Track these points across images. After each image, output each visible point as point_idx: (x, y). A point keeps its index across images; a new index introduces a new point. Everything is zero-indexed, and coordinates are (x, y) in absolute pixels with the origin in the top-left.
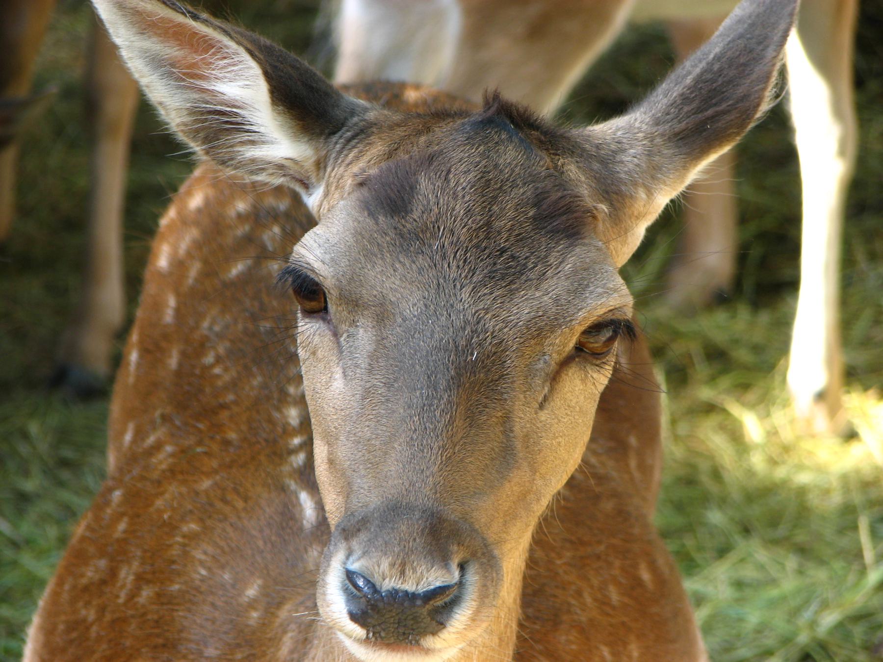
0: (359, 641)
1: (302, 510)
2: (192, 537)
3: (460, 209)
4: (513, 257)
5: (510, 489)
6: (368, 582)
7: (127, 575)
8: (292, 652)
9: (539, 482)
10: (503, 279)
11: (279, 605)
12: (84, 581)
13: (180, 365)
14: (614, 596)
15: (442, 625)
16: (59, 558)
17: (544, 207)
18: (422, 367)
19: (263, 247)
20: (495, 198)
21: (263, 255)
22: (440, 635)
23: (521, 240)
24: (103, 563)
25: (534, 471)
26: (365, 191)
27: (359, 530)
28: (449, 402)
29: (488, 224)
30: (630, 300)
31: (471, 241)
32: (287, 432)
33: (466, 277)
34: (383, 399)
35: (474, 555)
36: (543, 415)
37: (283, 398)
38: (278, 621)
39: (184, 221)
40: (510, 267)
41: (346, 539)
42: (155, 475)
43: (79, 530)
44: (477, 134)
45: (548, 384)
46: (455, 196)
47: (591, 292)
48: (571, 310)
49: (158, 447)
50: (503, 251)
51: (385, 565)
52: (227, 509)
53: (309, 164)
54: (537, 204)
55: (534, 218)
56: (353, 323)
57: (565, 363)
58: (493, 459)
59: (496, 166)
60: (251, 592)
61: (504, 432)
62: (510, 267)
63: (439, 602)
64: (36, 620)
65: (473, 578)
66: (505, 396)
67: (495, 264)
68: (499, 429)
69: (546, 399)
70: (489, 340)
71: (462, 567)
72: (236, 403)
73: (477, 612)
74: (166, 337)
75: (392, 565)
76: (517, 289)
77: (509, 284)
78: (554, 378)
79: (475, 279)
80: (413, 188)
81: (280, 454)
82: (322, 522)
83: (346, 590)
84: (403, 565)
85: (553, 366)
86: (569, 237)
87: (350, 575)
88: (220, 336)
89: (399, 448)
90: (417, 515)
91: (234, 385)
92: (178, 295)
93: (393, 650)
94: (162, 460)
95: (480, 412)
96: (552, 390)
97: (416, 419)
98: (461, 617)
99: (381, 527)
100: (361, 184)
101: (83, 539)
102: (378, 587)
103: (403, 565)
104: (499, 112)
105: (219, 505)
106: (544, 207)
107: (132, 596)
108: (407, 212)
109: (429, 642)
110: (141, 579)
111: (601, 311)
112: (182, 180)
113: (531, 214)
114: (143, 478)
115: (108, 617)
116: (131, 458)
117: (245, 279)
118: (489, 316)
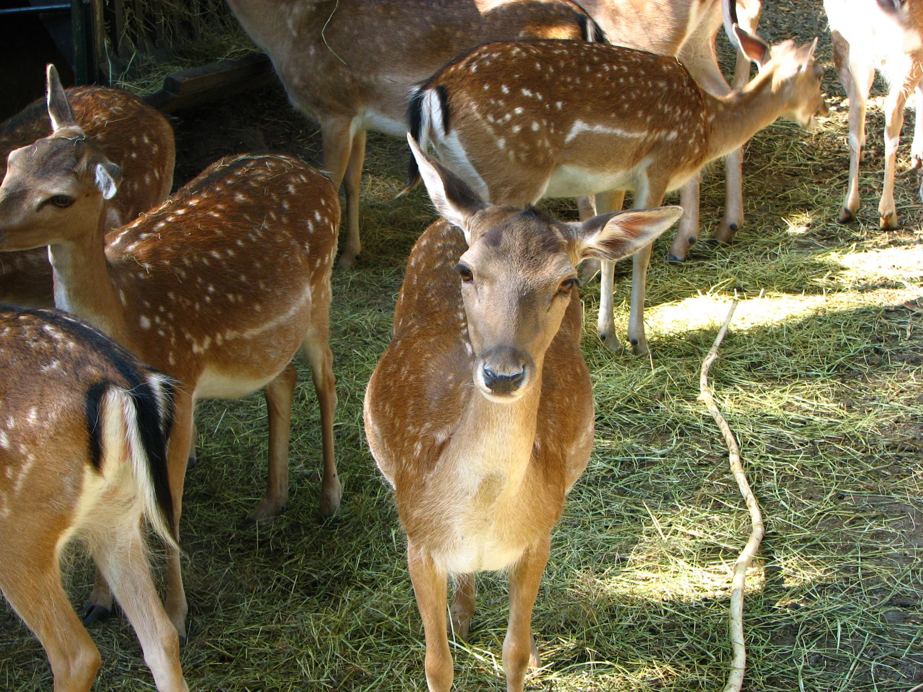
0: (489, 394)
1: (467, 350)
2: (428, 359)
3: (517, 244)
5: (538, 340)
6: (492, 373)
7: (404, 371)
8: (465, 398)
9: (547, 337)
11: (460, 382)
12: (389, 372)
13: (419, 298)
14: (569, 378)
15: (518, 387)
16: (378, 365)
19: (447, 257)
21: (447, 260)
24: (395, 366)
25: (546, 333)
26: (484, 238)
29: (527, 248)
30: (577, 273)
32: (459, 321)
35: (527, 362)
36: (549, 314)
37: (457, 310)
38: (460, 388)
39: (420, 250)
41: (483, 358)
42: (413, 335)
43: (384, 354)
46: (515, 239)
49: (413, 326)
50: (532, 258)
51: (498, 367)
52: (441, 349)
54: (543, 241)
55: (543, 246)
56: (482, 284)
57: (556, 295)
60: (450, 378)
63: (516, 380)
64: (369, 384)
65: (527, 371)
71: (524, 367)
72: (440, 311)
73: (529, 382)
74: (413, 289)
75: (500, 367)
78: (552, 301)
80: (501, 236)
81: (459, 329)
82: (474, 354)
83: (484, 376)
84: (504, 367)
85: (551, 297)
87: (485, 371)
88: (433, 288)
90: (508, 349)
91: (439, 304)
92: (418, 275)
94: (415, 330)
96: (551, 305)
98: (524, 384)
99: (496, 354)
100: (483, 236)
101: (387, 357)
103: (504, 367)
104: (530, 210)
105: (438, 348)
107: (406, 378)
109: (514, 393)
110: (410, 373)
112: (419, 236)
114: (408, 337)
115: (398, 385)
116: (403, 330)
117: (441, 268)
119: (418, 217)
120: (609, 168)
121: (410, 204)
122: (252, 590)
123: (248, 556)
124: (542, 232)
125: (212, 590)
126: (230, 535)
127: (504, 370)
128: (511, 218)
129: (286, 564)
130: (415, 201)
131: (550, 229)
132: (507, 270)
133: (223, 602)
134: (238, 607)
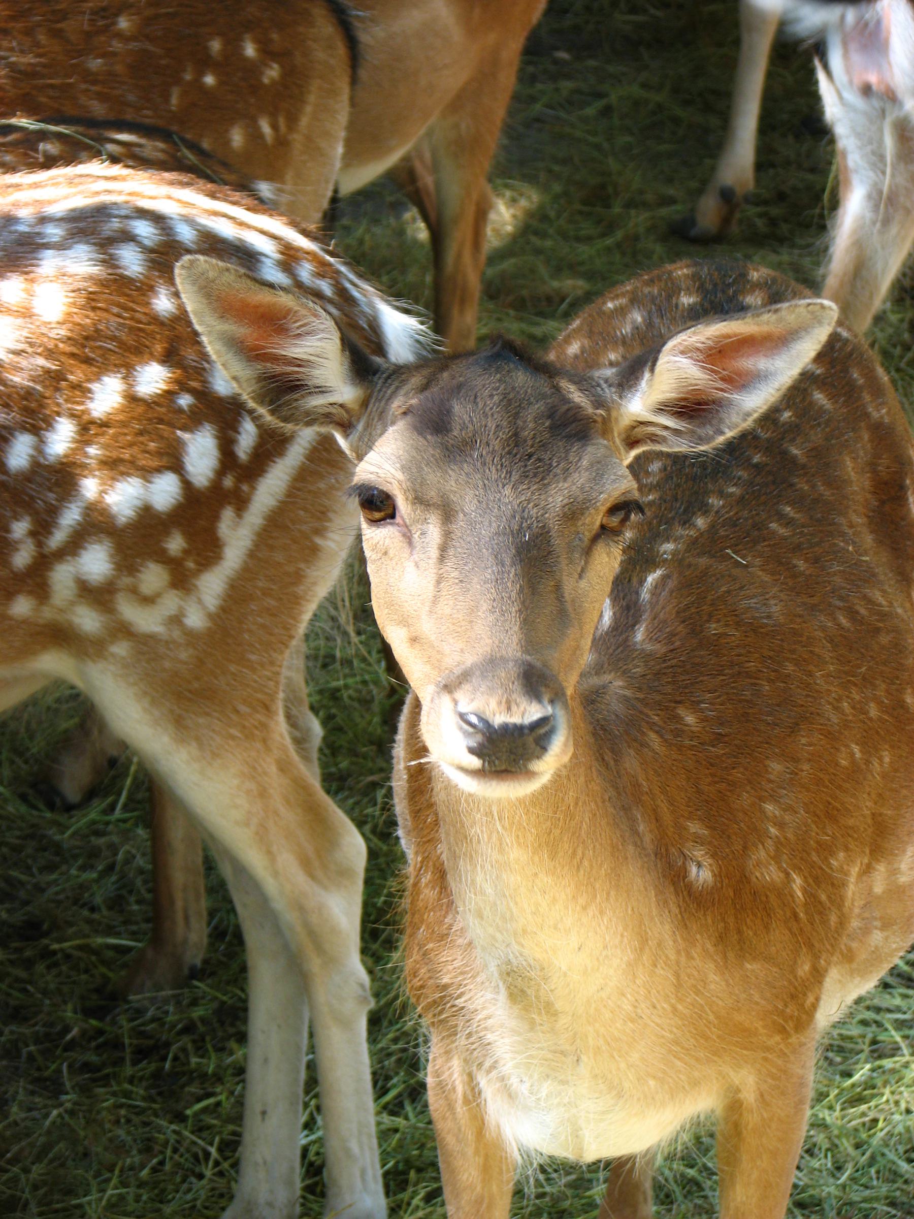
3: (492, 425)
4: (539, 460)
6: (481, 719)
10: (535, 476)
15: (544, 749)
17: (557, 418)
18: (487, 550)
20: (517, 414)
22: (544, 758)
23: (543, 446)
26: (409, 418)
27: (460, 683)
28: (516, 575)
29: (516, 434)
31: (504, 449)
33: (505, 478)
34: (457, 581)
36: (583, 584)
40: (539, 467)
44: (490, 366)
45: (584, 557)
47: (607, 479)
48: (594, 495)
50: (530, 456)
53: (354, 406)
54: (550, 417)
55: (551, 427)
57: (595, 539)
58: (553, 620)
59: (513, 388)
61: (557, 599)
62: (539, 467)
63: (542, 731)
66: (554, 569)
67: (526, 466)
68: (553, 596)
69: (583, 570)
70: (535, 525)
75: (499, 703)
76: (549, 484)
77: (542, 480)
78: (588, 552)
79: (513, 479)
80: (449, 412)
86: (579, 440)
89: (483, 616)
90: (511, 664)
93: (502, 780)
95: (539, 582)
96: (586, 562)
97: (493, 591)
102: (491, 722)
106: (557, 418)
108: (448, 431)
111: (616, 494)
113: (547, 424)
118: (530, 506)
119: (555, 284)
120: (7, 458)
121: (538, 252)
122: (114, 1165)
123: (105, 1081)
124: (544, 396)
125: (15, 1161)
126: (67, 1029)
127: (509, 709)
128: (463, 371)
129: (198, 1106)
130: (549, 243)
131: (557, 389)
132: (476, 487)
133: (42, 1192)
134: (80, 1206)
